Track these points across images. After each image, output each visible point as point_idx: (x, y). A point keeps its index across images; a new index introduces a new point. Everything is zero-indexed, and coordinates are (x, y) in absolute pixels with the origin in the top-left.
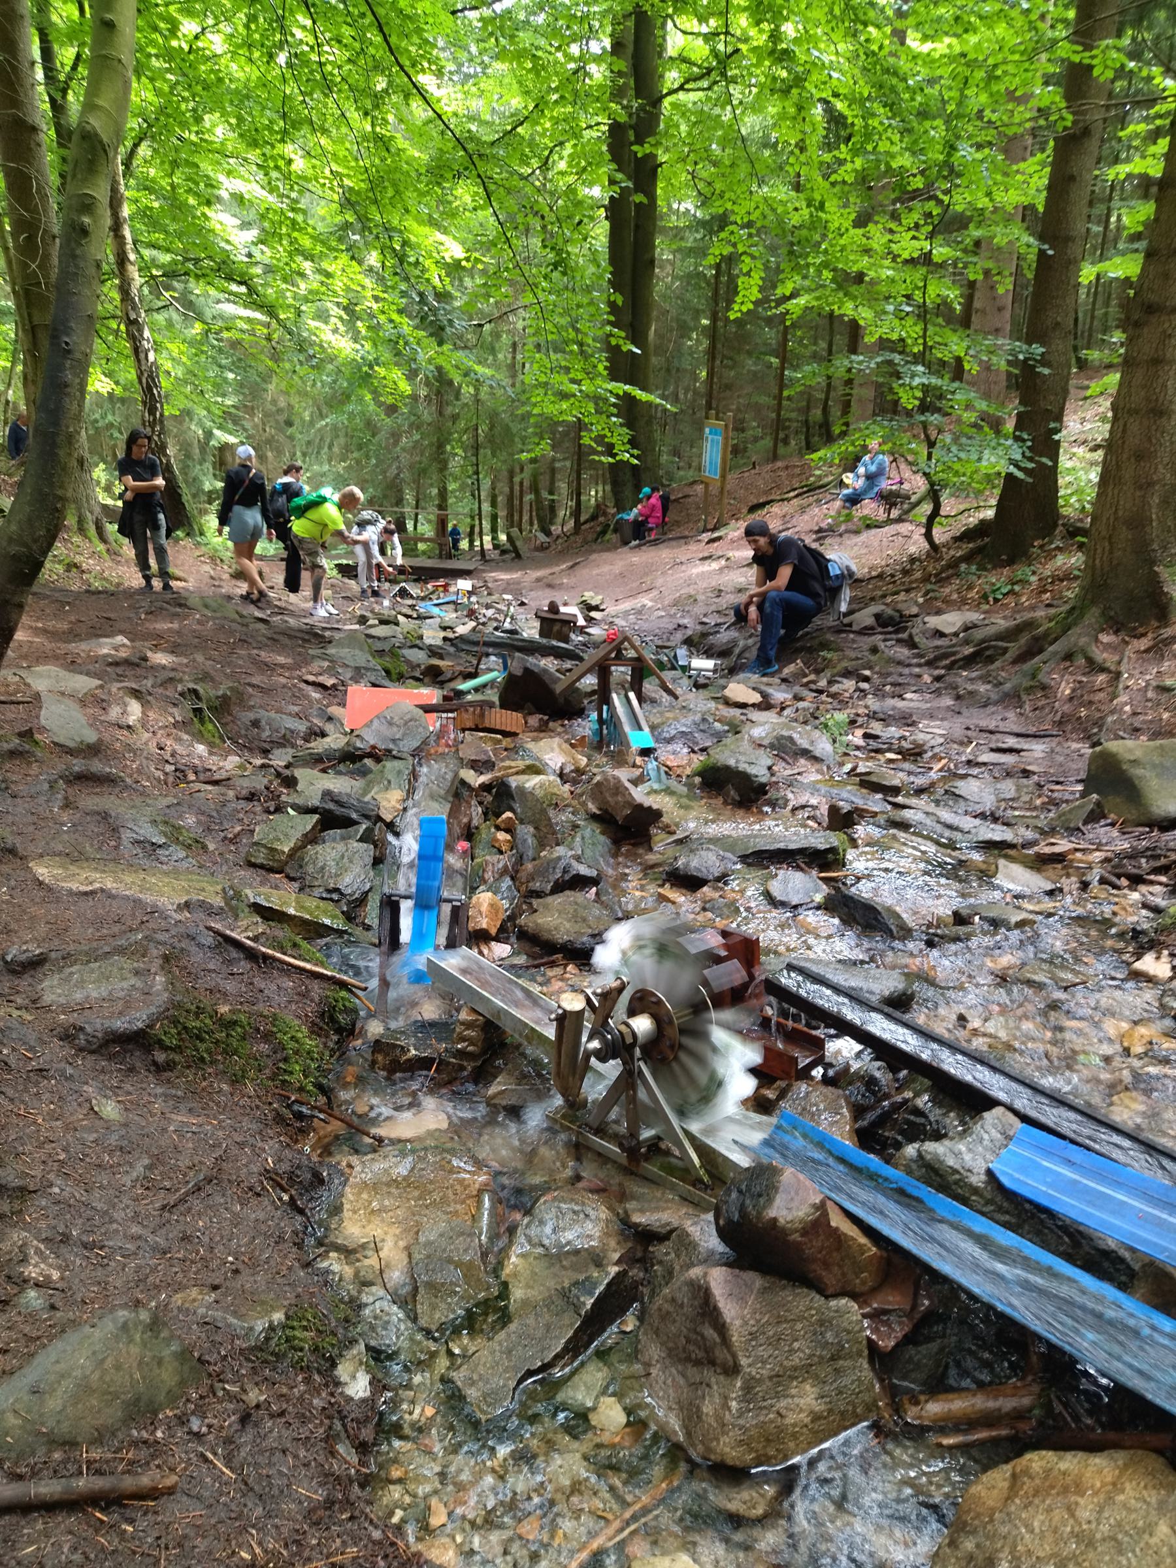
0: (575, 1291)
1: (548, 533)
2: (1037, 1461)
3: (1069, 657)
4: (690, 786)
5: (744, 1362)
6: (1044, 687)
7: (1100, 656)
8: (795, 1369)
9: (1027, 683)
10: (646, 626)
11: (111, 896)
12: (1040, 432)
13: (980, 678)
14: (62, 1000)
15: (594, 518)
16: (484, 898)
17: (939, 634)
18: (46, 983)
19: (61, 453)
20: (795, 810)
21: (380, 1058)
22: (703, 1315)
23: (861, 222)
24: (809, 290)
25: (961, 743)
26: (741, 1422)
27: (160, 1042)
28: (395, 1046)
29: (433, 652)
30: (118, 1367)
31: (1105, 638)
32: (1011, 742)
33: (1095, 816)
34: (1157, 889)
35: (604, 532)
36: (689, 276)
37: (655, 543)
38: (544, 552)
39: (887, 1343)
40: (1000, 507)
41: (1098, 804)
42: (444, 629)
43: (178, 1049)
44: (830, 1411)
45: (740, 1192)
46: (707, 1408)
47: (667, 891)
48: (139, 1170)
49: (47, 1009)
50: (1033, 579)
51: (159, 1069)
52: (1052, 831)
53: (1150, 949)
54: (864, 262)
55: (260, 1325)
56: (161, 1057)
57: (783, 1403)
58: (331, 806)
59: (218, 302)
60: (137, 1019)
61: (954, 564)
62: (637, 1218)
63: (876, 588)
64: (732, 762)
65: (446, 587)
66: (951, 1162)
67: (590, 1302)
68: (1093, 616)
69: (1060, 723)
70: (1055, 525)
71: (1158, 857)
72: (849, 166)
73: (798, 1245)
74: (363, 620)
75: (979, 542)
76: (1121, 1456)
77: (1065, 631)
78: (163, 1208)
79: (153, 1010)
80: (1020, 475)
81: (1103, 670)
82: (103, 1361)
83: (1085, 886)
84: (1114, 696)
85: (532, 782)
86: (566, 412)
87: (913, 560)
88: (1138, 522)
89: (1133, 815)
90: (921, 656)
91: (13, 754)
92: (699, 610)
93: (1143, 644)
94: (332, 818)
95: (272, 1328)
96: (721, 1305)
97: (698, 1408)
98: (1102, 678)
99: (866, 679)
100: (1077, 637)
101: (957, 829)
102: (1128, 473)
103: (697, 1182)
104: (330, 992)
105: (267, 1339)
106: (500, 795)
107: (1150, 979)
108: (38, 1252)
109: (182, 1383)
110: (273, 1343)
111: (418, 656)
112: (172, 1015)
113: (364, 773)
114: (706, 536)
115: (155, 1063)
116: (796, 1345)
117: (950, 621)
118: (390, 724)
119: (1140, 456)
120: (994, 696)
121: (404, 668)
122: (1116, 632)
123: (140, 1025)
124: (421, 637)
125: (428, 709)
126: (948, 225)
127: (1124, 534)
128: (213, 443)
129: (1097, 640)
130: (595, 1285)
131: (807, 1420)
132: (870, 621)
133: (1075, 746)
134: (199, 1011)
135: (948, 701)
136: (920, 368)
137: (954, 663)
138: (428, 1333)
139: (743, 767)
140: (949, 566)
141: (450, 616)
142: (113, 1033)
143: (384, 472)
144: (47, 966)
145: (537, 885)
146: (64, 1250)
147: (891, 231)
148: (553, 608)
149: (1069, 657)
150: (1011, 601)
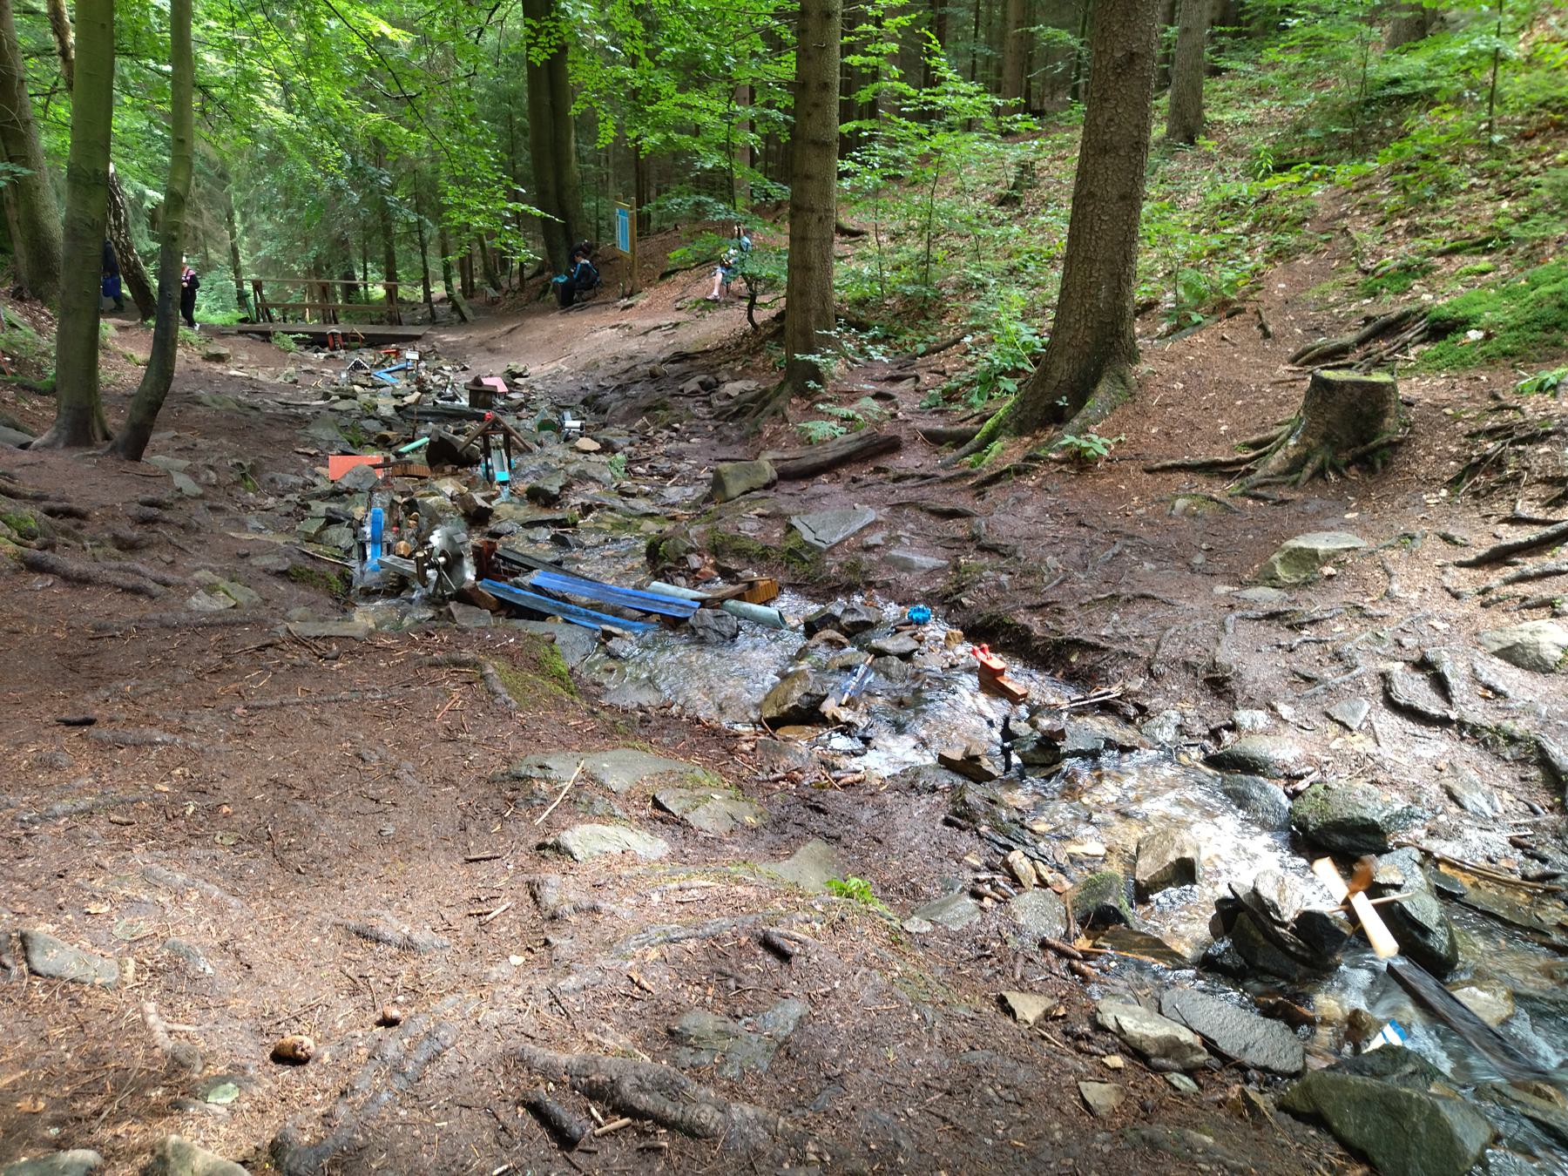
1: (497, 287)
3: (775, 413)
4: (521, 499)
10: (558, 389)
16: (402, 543)
29: (387, 423)
31: (794, 401)
35: (545, 292)
37: (581, 308)
38: (492, 311)
42: (396, 396)
60: (284, 567)
65: (397, 353)
68: (787, 389)
74: (326, 396)
85: (431, 500)
92: (599, 374)
94: (332, 520)
99: (676, 430)
106: (412, 506)
111: (372, 425)
113: (344, 500)
121: (363, 436)
124: (376, 407)
125: (376, 467)
128: (147, 204)
141: (401, 385)
143: (328, 230)
148: (477, 381)
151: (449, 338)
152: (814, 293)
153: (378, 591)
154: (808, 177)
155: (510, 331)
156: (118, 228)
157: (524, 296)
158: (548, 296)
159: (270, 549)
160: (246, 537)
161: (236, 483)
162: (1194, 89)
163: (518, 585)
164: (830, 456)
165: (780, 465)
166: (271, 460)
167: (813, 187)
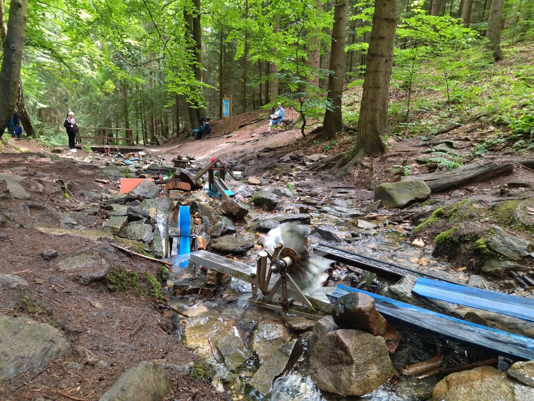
0: (284, 349)
2: (453, 376)
3: (356, 164)
5: (355, 359)
6: (349, 174)
7: (365, 164)
8: (370, 360)
9: (343, 173)
11: (71, 237)
12: (335, 97)
13: (328, 173)
14: (68, 269)
15: (183, 132)
17: (312, 161)
18: (59, 264)
19: (12, 89)
20: (287, 211)
21: (178, 291)
22: (336, 346)
23: (275, 31)
24: (259, 53)
25: (328, 192)
26: (357, 380)
27: (110, 281)
28: (183, 286)
30: (148, 382)
31: (366, 158)
32: (343, 190)
33: (380, 207)
34: (407, 224)
35: (188, 136)
36: (212, 52)
39: (393, 351)
40: (325, 123)
41: (381, 203)
43: (116, 284)
44: (382, 373)
45: (342, 304)
46: (343, 378)
47: (257, 233)
48: (117, 323)
49: (63, 272)
50: (337, 144)
51: (110, 291)
52: (368, 212)
53: (415, 238)
54: (276, 45)
55: (187, 367)
56: (111, 287)
57: (368, 372)
58: (131, 213)
59: (38, 56)
60: (100, 273)
61: (311, 140)
62: (295, 325)
63: (287, 149)
64: (264, 196)
66: (400, 291)
67: (291, 351)
68: (361, 152)
69: (356, 184)
70: (342, 127)
71: (405, 215)
72: (271, 13)
73: (368, 316)
75: (318, 134)
76: (480, 369)
77: (353, 157)
78: (130, 336)
79: (105, 269)
80: (332, 110)
81: (367, 168)
82: (143, 379)
83: (385, 225)
84: (372, 175)
86: (180, 91)
87: (298, 140)
88: (373, 122)
89: (392, 205)
90: (308, 168)
91: (4, 198)
92: (228, 159)
93: (378, 159)
94: (132, 218)
95: (191, 368)
96: (344, 341)
97: (340, 379)
98: (367, 170)
100: (358, 158)
101: (342, 212)
102: (369, 107)
103: (312, 312)
104: (160, 266)
105: (190, 371)
107: (418, 246)
108: (89, 353)
109: (167, 388)
110: (192, 373)
112: (112, 271)
114: (226, 136)
115: (109, 289)
116: (369, 352)
117: (315, 157)
118: (144, 187)
119: (372, 101)
120: (334, 178)
122: (369, 157)
123: (103, 275)
126: (303, 33)
127: (369, 126)
128: (38, 107)
129: (363, 159)
130: (291, 346)
131: (376, 377)
132: (289, 158)
133: (363, 190)
134: (121, 271)
135: (319, 180)
136: (298, 78)
137: (319, 169)
138: (233, 371)
139: (268, 198)
140: (310, 141)
142: (93, 278)
143: (104, 117)
144: (58, 258)
145: (215, 234)
146: (97, 352)
147: (285, 34)
149: (356, 164)
150: (331, 151)
151: (154, 150)
152: (380, 101)
153: (195, 291)
154: (382, 38)
155: (179, 147)
156: (19, 97)
157: (179, 139)
158: (190, 138)
159: (80, 248)
160: (56, 232)
161: (58, 193)
162: (498, 36)
163: (395, 295)
164: (460, 178)
165: (432, 183)
166: (81, 184)
167: (383, 44)
